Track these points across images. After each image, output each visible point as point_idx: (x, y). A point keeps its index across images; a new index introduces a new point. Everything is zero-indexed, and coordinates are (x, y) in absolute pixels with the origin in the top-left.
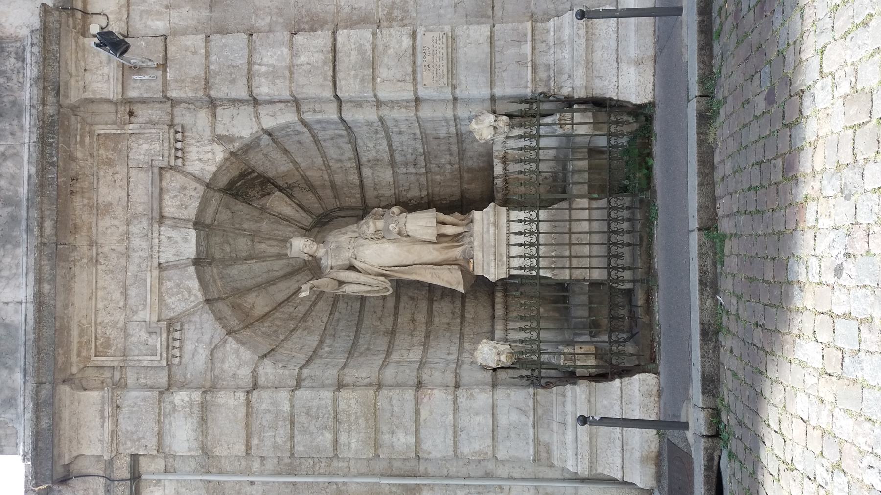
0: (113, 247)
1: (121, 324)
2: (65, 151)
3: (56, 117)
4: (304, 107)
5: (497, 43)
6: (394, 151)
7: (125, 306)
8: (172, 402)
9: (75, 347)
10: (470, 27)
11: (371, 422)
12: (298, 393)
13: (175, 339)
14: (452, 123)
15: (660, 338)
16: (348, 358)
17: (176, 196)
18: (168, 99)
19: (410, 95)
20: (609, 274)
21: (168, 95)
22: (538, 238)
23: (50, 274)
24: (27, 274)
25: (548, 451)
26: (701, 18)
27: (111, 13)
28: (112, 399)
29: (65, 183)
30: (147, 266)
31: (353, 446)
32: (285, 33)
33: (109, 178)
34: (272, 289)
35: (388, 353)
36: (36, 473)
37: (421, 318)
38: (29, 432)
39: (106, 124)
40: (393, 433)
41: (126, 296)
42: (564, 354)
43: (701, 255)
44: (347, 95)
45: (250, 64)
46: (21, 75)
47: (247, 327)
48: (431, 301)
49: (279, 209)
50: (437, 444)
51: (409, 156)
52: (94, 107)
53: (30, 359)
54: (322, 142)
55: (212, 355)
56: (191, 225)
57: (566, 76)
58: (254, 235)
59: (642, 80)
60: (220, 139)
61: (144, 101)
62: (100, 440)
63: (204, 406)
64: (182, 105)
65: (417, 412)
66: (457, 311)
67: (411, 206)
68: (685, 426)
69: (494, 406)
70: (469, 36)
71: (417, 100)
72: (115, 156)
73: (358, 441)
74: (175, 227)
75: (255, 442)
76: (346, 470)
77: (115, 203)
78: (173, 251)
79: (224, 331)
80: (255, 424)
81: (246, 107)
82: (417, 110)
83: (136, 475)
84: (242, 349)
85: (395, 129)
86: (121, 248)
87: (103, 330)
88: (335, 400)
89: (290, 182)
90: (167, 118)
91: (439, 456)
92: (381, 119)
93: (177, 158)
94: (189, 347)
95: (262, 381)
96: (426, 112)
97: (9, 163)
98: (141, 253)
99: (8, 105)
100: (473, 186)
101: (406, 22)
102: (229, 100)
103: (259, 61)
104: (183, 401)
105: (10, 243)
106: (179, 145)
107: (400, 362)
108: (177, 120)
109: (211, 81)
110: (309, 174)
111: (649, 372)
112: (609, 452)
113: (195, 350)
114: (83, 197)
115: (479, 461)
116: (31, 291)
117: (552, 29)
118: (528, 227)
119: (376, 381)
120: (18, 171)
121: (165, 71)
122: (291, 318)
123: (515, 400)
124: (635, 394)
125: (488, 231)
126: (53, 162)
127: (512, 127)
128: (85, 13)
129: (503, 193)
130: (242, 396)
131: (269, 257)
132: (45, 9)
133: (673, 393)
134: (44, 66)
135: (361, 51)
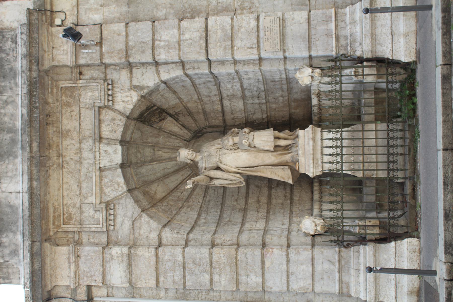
0: (72, 157)
1: (78, 205)
2: (43, 99)
3: (38, 79)
4: (187, 66)
5: (312, 23)
6: (245, 89)
7: (80, 194)
8: (110, 254)
9: (51, 219)
10: (295, 13)
11: (234, 268)
12: (187, 249)
13: (110, 215)
14: (283, 72)
15: (421, 215)
16: (217, 227)
17: (109, 125)
18: (103, 64)
19: (256, 57)
20: (389, 174)
21: (104, 62)
22: (342, 151)
23: (37, 175)
24: (22, 175)
25: (348, 288)
26: (443, 15)
27: (67, 11)
28: (75, 251)
29: (43, 118)
30: (93, 169)
31: (223, 283)
32: (175, 20)
33: (68, 114)
34: (167, 181)
35: (243, 224)
36: (33, 296)
37: (264, 199)
38: (28, 270)
39: (66, 80)
40: (248, 276)
41: (80, 188)
42: (359, 226)
43: (445, 166)
44: (215, 58)
45: (153, 40)
46: (15, 52)
47: (153, 206)
48: (270, 188)
49: (170, 128)
50: (276, 283)
51: (254, 92)
52: (58, 70)
53: (27, 227)
54: (198, 86)
55: (133, 224)
56: (118, 143)
57: (358, 44)
58: (155, 146)
59: (408, 46)
60: (135, 88)
61: (88, 66)
62: (68, 276)
63: (129, 256)
64: (111, 67)
65: (263, 262)
66: (288, 195)
67: (257, 126)
68: (434, 273)
69: (313, 259)
70: (293, 19)
71: (260, 59)
72: (71, 101)
73: (225, 280)
74: (109, 144)
75: (161, 279)
76: (219, 297)
77: (72, 129)
78: (108, 159)
79: (140, 210)
80: (161, 268)
81: (151, 67)
82: (260, 66)
83: (90, 298)
84: (151, 221)
85: (246, 77)
86: (77, 158)
87: (67, 209)
88: (211, 255)
89: (177, 111)
90: (102, 76)
91: (277, 290)
92: (237, 72)
93: (109, 100)
94: (119, 219)
95: (164, 241)
96: (266, 67)
97: (10, 107)
98: (88, 161)
99: (8, 71)
100: (298, 111)
101: (253, 10)
102: (140, 63)
103: (159, 39)
104: (117, 253)
105: (11, 155)
106: (110, 92)
107: (251, 230)
108: (109, 77)
109: (129, 52)
110: (189, 105)
111: (414, 237)
112: (387, 287)
113: (123, 221)
114: (53, 127)
115: (303, 294)
116: (26, 186)
117: (348, 13)
118: (335, 143)
119: (236, 242)
120: (15, 112)
121: (101, 47)
122: (179, 200)
123: (327, 254)
124: (403, 252)
125: (308, 144)
126: (37, 106)
127: (323, 76)
128: (52, 12)
129: (318, 116)
130: (153, 250)
131: (164, 160)
132: (29, 12)
133: (427, 252)
134: (30, 47)
135: (223, 30)
